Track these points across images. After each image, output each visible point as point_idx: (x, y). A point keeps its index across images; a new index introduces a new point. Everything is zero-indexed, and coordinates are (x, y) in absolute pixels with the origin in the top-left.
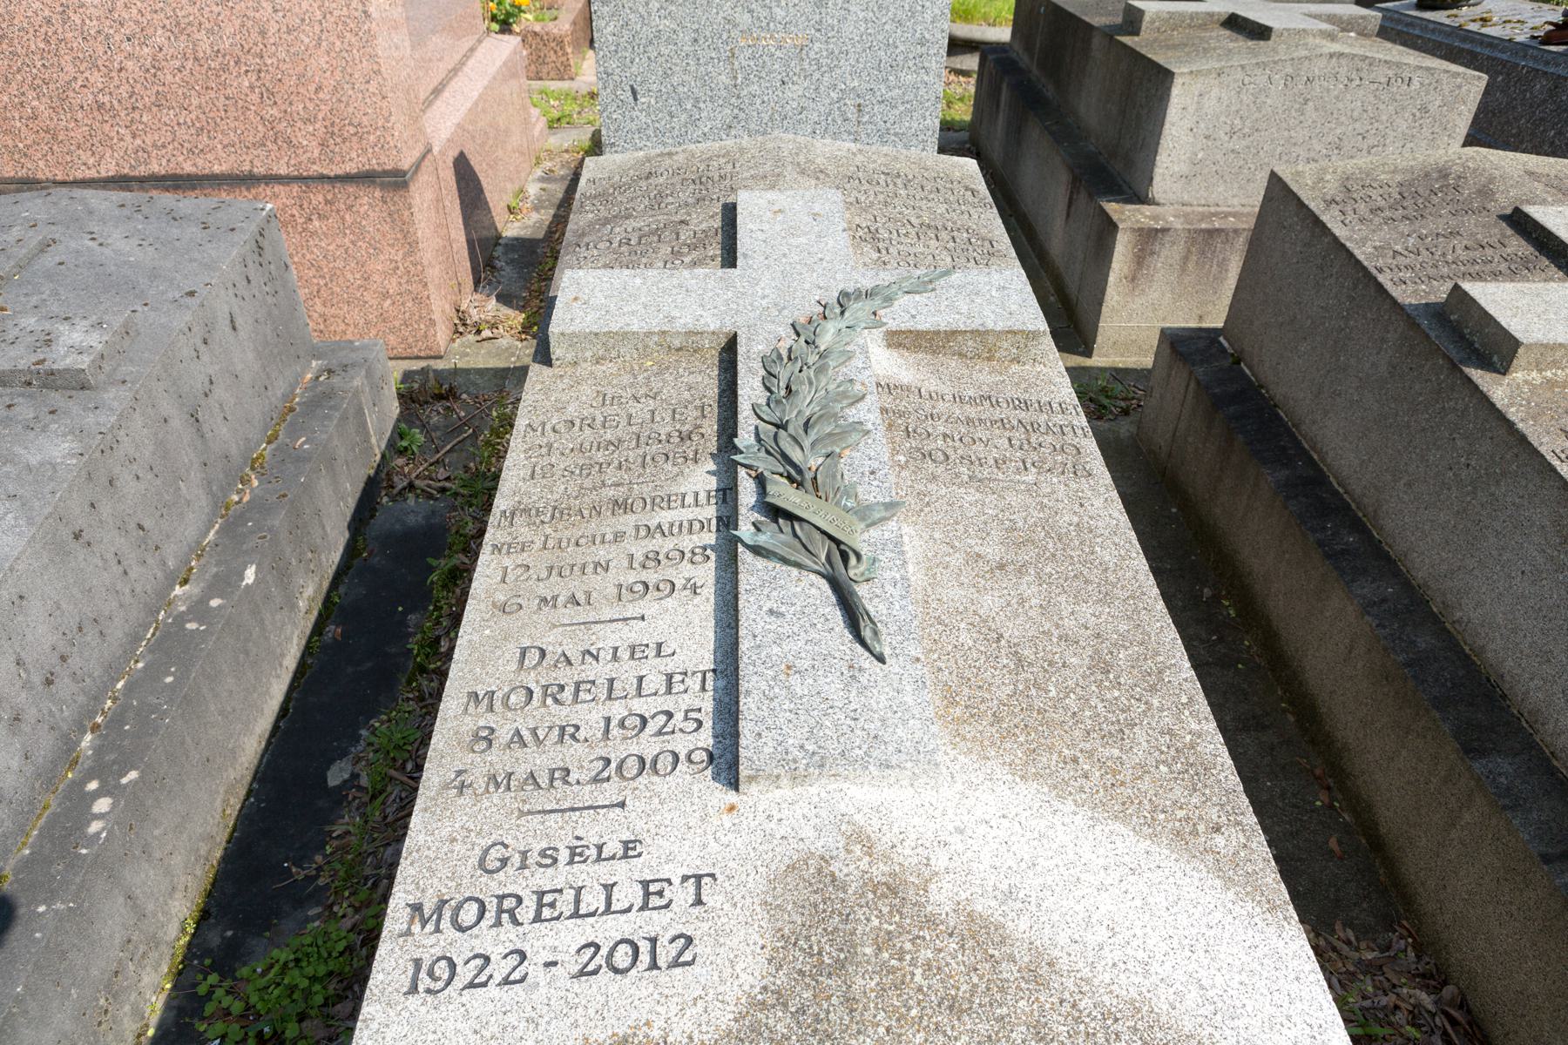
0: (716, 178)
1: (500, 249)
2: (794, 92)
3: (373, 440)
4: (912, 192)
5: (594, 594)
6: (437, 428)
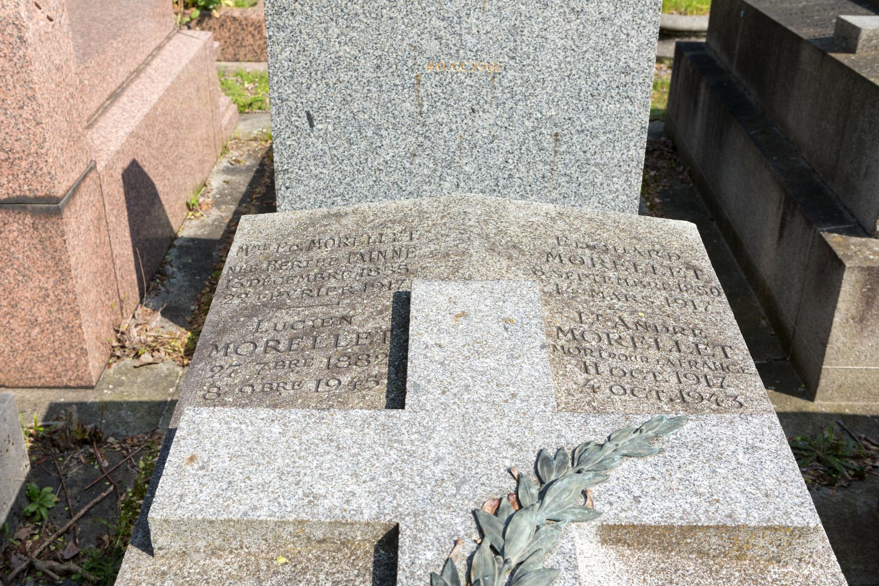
0: (390, 254)
1: (174, 252)
2: (485, 120)
4: (624, 274)
6: (74, 483)
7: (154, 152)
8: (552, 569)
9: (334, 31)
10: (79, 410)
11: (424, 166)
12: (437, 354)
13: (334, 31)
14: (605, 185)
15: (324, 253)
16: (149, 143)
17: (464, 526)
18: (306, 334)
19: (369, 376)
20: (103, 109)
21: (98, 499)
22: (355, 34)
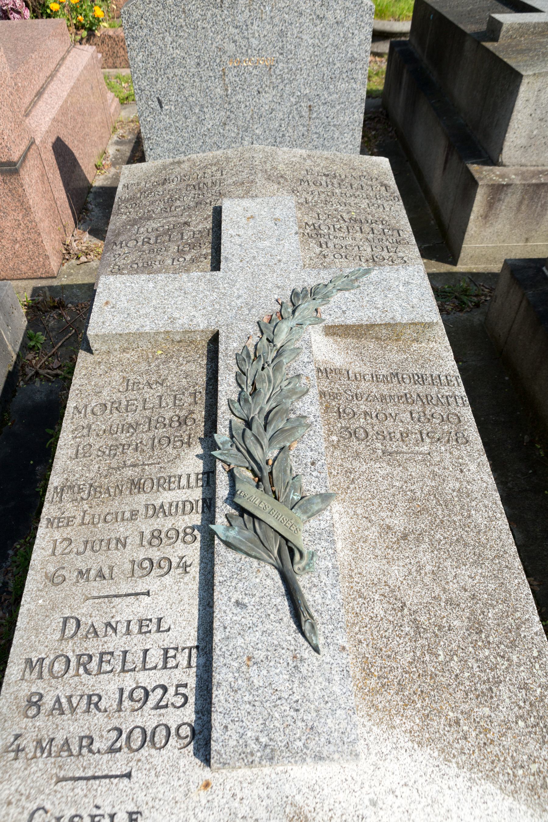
0: (210, 184)
1: (91, 195)
2: (267, 98)
3: (10, 348)
4: (344, 190)
5: (116, 570)
6: (53, 330)
7: (70, 132)
8: (299, 348)
9: (169, 39)
10: (49, 290)
11: (232, 131)
12: (237, 240)
13: (169, 39)
14: (340, 139)
15: (172, 186)
16: (66, 125)
17: (253, 329)
18: (165, 233)
19: (201, 255)
20: (33, 103)
21: (67, 337)
22: (182, 41)
